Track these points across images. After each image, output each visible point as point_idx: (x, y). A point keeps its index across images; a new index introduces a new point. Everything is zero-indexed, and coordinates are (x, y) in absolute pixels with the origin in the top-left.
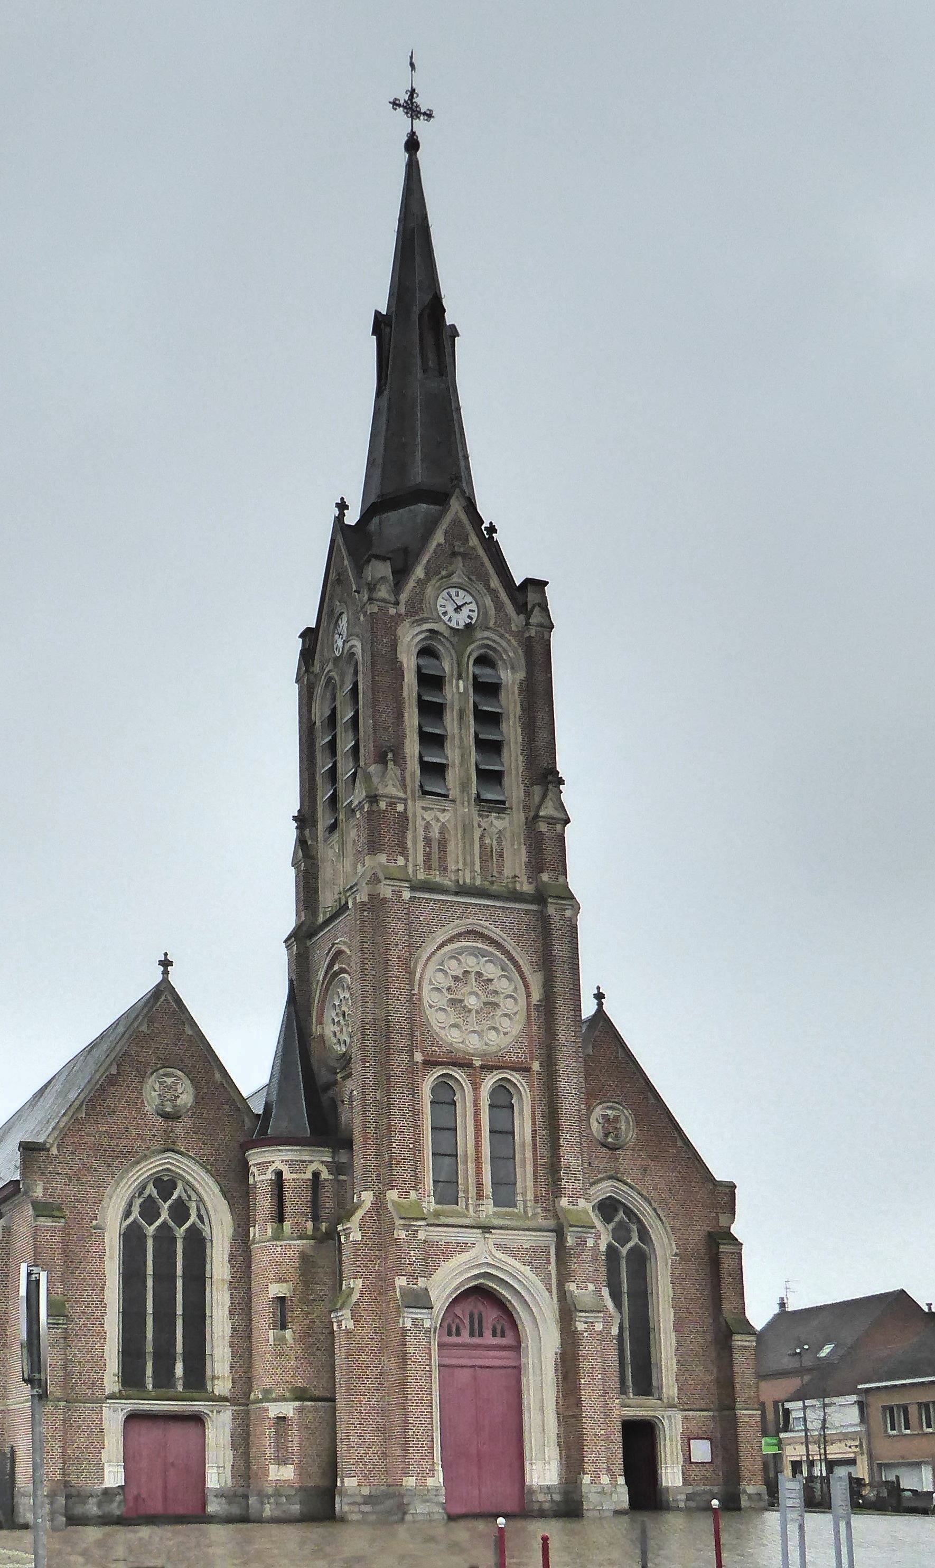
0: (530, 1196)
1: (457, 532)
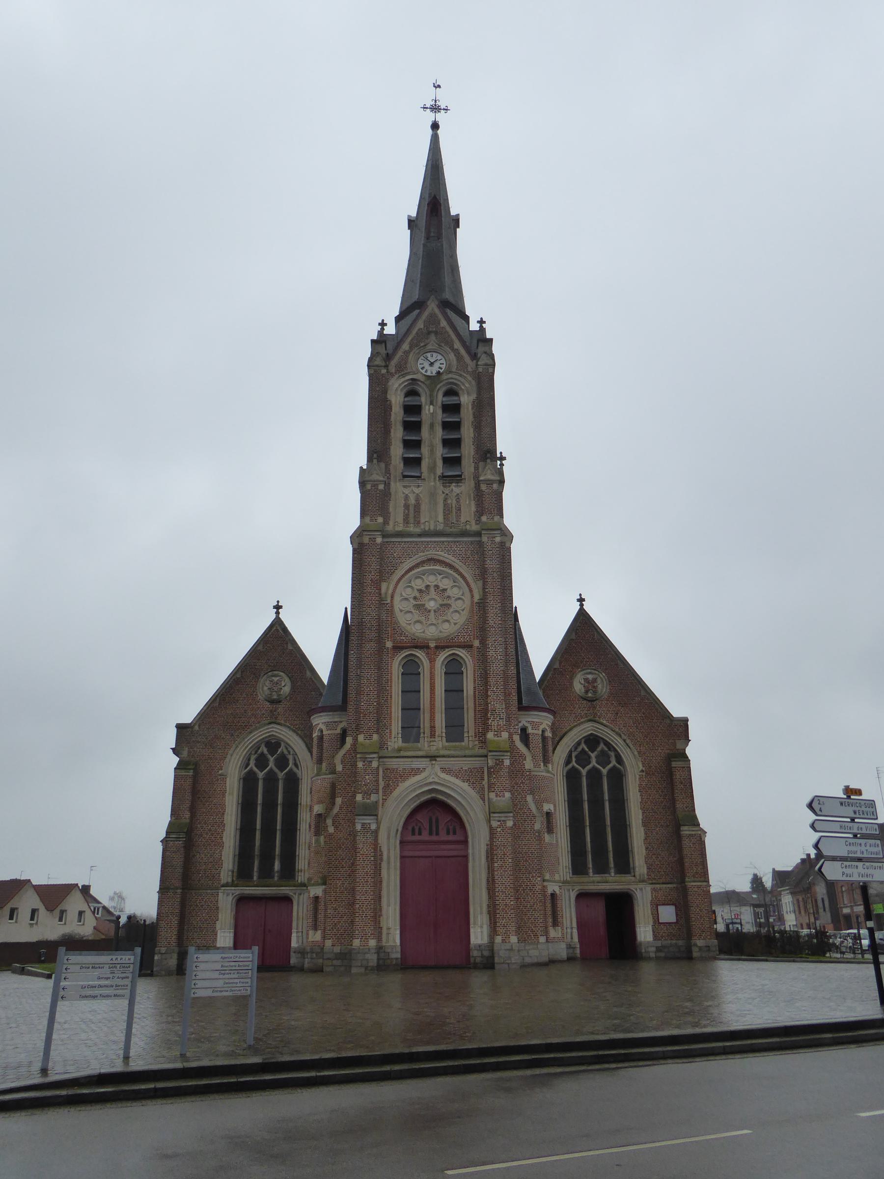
0: (472, 733)
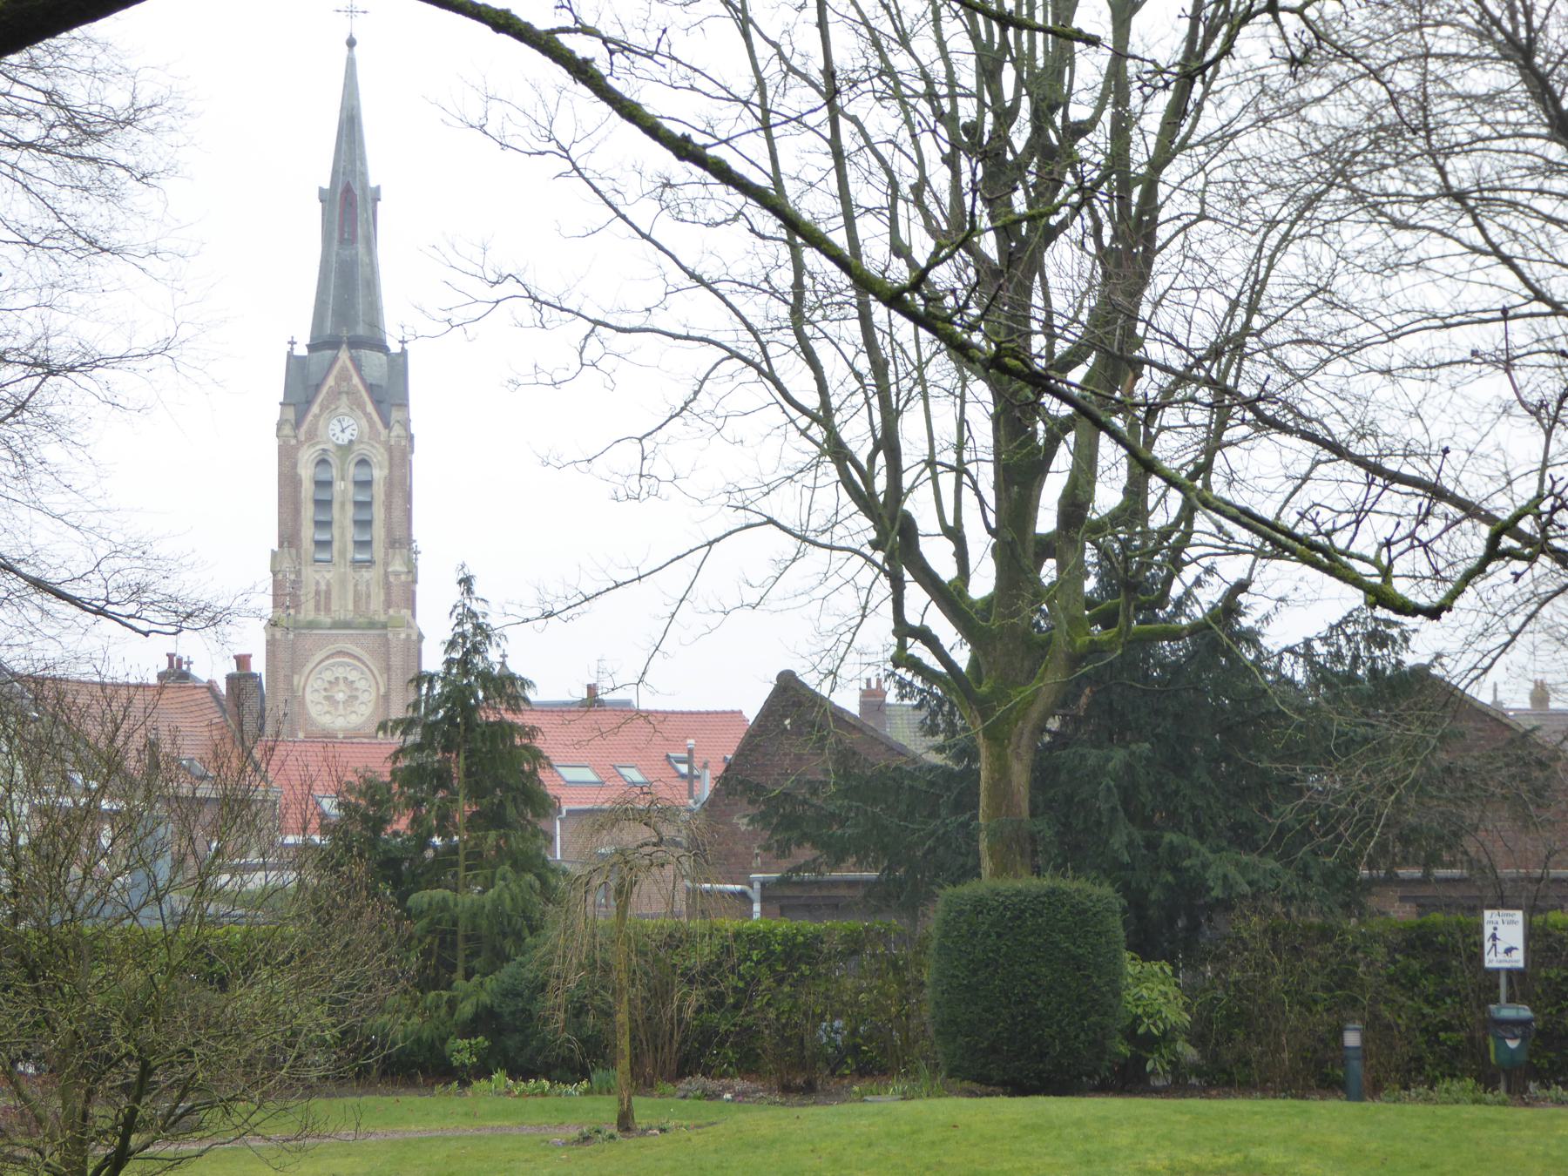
1: (344, 377)
